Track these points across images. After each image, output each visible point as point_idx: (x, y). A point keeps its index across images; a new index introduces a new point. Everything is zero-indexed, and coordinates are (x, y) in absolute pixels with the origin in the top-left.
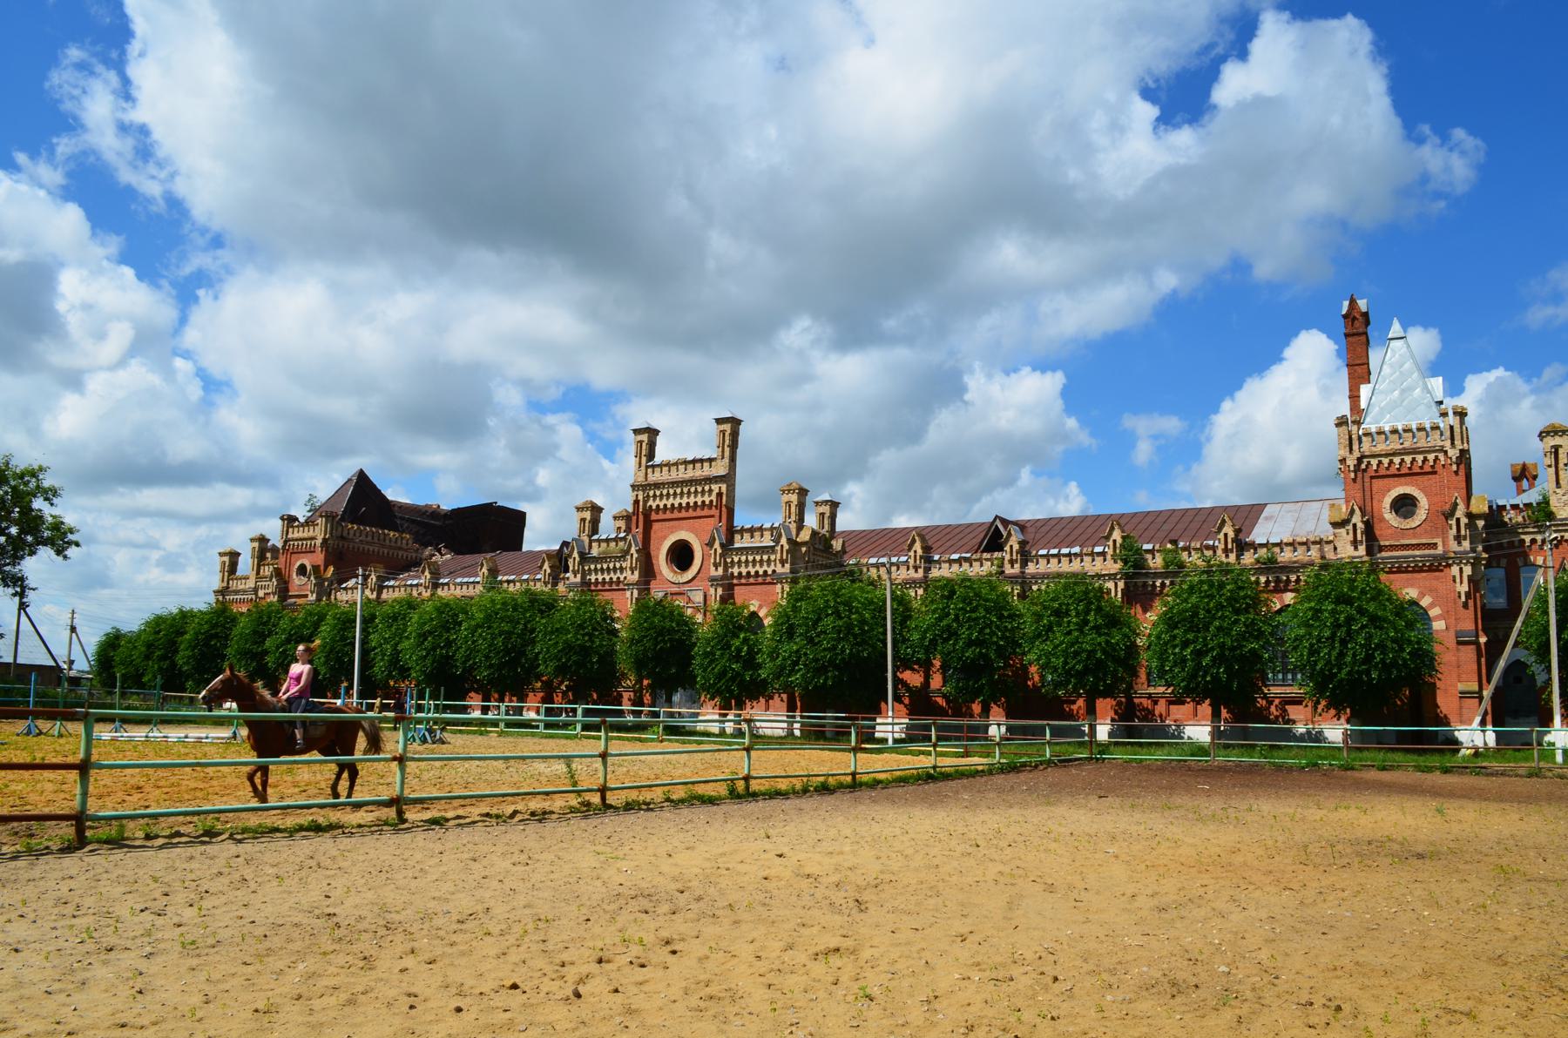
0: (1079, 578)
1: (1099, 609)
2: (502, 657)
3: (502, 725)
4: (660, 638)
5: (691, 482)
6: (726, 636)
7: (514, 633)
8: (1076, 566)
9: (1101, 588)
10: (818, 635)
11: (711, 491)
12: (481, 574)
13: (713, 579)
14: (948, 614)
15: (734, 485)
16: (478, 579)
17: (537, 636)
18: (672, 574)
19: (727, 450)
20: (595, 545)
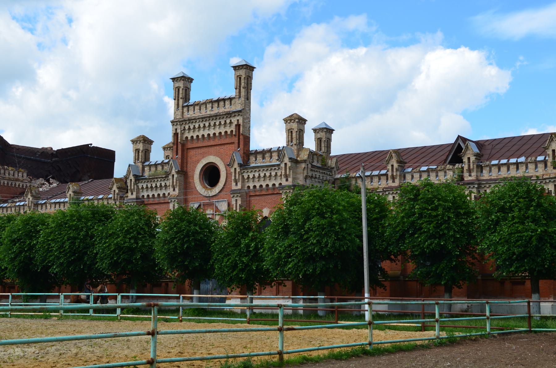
0: (522, 181)
1: (539, 205)
2: (69, 257)
3: (119, 311)
4: (186, 239)
5: (216, 116)
6: (238, 236)
7: (78, 238)
8: (521, 173)
9: (543, 189)
10: (307, 232)
11: (231, 123)
12: (27, 200)
13: (234, 192)
14: (414, 214)
15: (249, 118)
16: (67, 200)
17: (95, 240)
18: (204, 190)
19: (243, 90)
20: (147, 169)
